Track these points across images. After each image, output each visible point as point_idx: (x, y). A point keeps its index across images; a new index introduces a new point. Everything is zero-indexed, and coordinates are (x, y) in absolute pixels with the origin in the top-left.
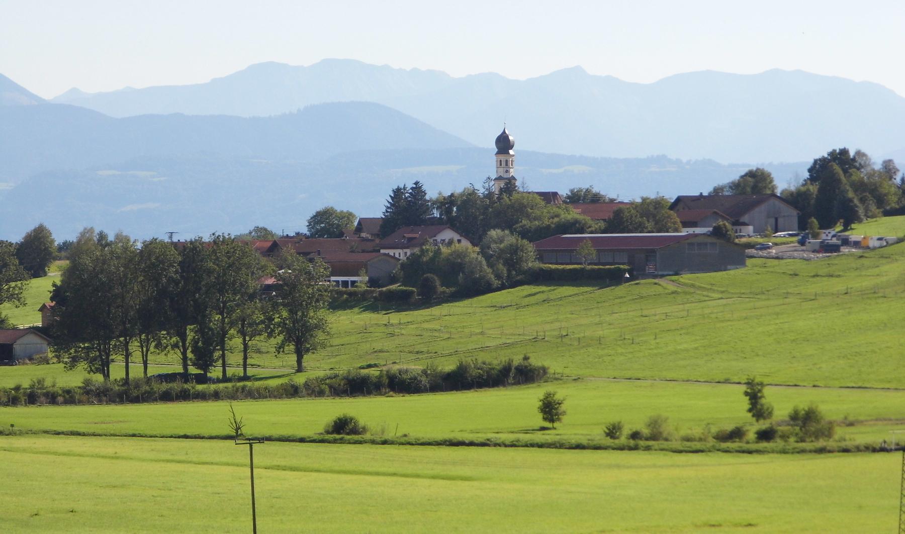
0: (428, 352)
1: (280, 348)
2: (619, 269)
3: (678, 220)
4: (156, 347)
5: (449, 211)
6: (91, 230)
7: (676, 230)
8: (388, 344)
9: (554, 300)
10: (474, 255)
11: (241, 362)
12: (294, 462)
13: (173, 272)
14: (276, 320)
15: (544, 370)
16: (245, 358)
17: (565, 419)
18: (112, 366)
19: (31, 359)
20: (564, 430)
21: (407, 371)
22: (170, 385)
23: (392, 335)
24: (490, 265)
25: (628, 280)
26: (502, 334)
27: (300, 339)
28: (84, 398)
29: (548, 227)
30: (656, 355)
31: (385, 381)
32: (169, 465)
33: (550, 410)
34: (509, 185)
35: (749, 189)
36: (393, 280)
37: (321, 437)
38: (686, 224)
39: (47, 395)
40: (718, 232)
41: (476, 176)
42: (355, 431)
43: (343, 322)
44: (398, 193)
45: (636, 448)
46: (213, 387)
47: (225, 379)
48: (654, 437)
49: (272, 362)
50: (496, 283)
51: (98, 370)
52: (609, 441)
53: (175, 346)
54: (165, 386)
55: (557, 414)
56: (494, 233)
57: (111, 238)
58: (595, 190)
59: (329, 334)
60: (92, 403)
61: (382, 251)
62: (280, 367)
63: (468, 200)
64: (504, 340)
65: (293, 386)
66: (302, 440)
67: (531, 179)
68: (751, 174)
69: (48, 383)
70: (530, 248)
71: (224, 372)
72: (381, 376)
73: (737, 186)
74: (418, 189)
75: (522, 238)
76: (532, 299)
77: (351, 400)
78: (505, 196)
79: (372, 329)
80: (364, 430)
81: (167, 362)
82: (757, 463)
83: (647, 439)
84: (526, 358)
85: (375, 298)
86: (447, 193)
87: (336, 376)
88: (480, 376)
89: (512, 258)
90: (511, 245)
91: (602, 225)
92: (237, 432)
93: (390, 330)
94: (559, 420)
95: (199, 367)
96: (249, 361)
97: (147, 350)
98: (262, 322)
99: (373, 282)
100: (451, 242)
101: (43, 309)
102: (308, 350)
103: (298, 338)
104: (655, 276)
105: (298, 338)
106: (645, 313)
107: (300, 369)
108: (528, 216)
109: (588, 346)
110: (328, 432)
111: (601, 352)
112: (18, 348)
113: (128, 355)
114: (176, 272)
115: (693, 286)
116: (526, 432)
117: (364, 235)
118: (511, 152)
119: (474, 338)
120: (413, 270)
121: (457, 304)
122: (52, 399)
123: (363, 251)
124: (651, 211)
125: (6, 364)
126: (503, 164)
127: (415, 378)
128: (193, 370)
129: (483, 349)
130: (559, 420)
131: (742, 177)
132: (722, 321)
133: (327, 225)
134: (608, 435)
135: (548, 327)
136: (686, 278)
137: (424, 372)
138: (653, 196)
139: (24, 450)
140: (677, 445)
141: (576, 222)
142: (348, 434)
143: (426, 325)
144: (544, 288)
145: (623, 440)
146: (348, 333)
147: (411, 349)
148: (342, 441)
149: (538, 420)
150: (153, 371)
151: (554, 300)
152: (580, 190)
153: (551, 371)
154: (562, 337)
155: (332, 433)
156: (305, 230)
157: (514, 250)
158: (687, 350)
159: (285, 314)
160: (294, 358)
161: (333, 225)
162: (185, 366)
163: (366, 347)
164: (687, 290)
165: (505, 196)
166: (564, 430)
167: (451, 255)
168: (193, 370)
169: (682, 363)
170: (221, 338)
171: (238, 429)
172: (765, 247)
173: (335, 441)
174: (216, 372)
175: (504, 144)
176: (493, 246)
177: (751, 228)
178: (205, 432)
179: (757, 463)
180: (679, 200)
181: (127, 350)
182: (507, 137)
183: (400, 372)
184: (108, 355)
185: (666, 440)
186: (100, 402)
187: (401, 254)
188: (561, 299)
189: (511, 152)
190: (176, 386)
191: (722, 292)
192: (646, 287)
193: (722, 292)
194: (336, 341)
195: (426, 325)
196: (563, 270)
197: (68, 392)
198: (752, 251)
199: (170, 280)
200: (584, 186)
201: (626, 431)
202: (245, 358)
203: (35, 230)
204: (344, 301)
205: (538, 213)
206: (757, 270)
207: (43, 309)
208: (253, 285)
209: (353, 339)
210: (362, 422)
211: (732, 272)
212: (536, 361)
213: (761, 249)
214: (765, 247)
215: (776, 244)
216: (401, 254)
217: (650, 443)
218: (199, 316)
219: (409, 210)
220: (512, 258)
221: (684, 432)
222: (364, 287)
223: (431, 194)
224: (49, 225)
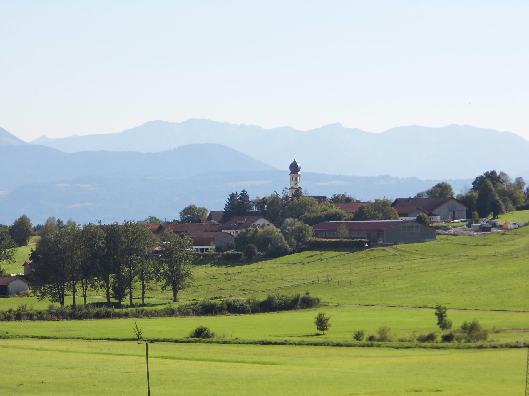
0: (250, 290)
1: (164, 288)
2: (362, 241)
3: (396, 213)
4: (91, 287)
5: (262, 207)
6: (53, 219)
7: (395, 219)
8: (227, 285)
9: (324, 259)
10: (277, 233)
11: (141, 296)
12: (172, 354)
13: (101, 243)
14: (161, 271)
15: (318, 300)
16: (143, 293)
17: (330, 329)
19: (18, 294)
20: (330, 335)
22: (100, 309)
23: (229, 280)
24: (287, 239)
25: (367, 248)
27: (175, 282)
28: (49, 316)
29: (321, 216)
31: (225, 306)
33: (322, 324)
34: (298, 192)
35: (438, 195)
36: (230, 248)
37: (187, 339)
38: (401, 215)
39: (27, 315)
40: (420, 220)
41: (278, 187)
42: (207, 336)
43: (201, 272)
45: (372, 346)
47: (132, 306)
48: (382, 339)
49: (159, 295)
50: (290, 249)
52: (356, 342)
53: (102, 286)
54: (96, 310)
55: (325, 326)
56: (289, 220)
57: (65, 223)
58: (348, 195)
59: (192, 279)
60: (53, 319)
61: (223, 231)
63: (274, 201)
65: (171, 310)
66: (177, 341)
67: (310, 189)
70: (310, 229)
71: (131, 301)
72: (222, 304)
74: (244, 195)
75: (305, 223)
77: (205, 318)
78: (295, 198)
79: (217, 276)
80: (213, 335)
81: (98, 295)
82: (442, 355)
83: (378, 341)
84: (307, 293)
85: (219, 258)
86: (261, 197)
87: (196, 304)
88: (281, 304)
89: (299, 235)
91: (352, 215)
92: (139, 336)
93: (228, 277)
94: (327, 329)
95: (116, 299)
96: (146, 295)
97: (86, 289)
98: (153, 272)
99: (218, 249)
100: (263, 226)
101: (25, 264)
102: (180, 289)
106: (377, 267)
108: (309, 210)
109: (344, 286)
111: (351, 290)
112: (10, 287)
113: (75, 292)
114: (103, 243)
115: (405, 251)
116: (308, 336)
117: (212, 221)
118: (299, 173)
119: (277, 282)
120: (242, 242)
121: (267, 262)
122: (30, 317)
123: (212, 231)
124: (381, 207)
125: (3, 297)
126: (294, 180)
127: (243, 305)
128: (113, 300)
130: (327, 329)
131: (434, 187)
133: (191, 215)
136: (401, 246)
137: (248, 301)
138: (381, 199)
139: (14, 347)
141: (337, 214)
142: (203, 338)
143: (249, 274)
144: (318, 252)
145: (364, 341)
147: (240, 288)
148: (200, 342)
149: (315, 330)
150: (89, 301)
151: (324, 259)
152: (339, 195)
153: (322, 301)
154: (329, 281)
155: (194, 337)
156: (178, 219)
157: (301, 230)
158: (401, 289)
159: (167, 268)
162: (108, 298)
163: (214, 287)
165: (295, 198)
166: (330, 335)
167: (264, 233)
168: (113, 300)
170: (129, 282)
171: (139, 334)
172: (447, 229)
173: (196, 342)
174: (126, 301)
175: (294, 168)
176: (288, 228)
177: (439, 217)
179: (442, 355)
180: (397, 201)
181: (74, 288)
182: (297, 164)
183: (234, 301)
184: (63, 292)
185: (390, 341)
186: (59, 319)
187: (235, 233)
188: (328, 259)
189: (299, 173)
190: (103, 310)
191: (422, 255)
192: (377, 251)
194: (196, 284)
195: (249, 274)
196: (329, 242)
197: (40, 313)
198: (440, 231)
199: (100, 248)
200: (342, 193)
201: (366, 336)
202: (143, 293)
203: (20, 219)
204: (201, 260)
206: (442, 241)
207: (25, 264)
209: (206, 282)
211: (428, 243)
212: (313, 295)
213: (445, 230)
214: (447, 229)
215: (454, 227)
216: (235, 233)
217: (380, 343)
218: (116, 269)
219: (239, 207)
220: (299, 235)
221: (400, 336)
222: (213, 252)
223: (252, 197)
224: (28, 216)
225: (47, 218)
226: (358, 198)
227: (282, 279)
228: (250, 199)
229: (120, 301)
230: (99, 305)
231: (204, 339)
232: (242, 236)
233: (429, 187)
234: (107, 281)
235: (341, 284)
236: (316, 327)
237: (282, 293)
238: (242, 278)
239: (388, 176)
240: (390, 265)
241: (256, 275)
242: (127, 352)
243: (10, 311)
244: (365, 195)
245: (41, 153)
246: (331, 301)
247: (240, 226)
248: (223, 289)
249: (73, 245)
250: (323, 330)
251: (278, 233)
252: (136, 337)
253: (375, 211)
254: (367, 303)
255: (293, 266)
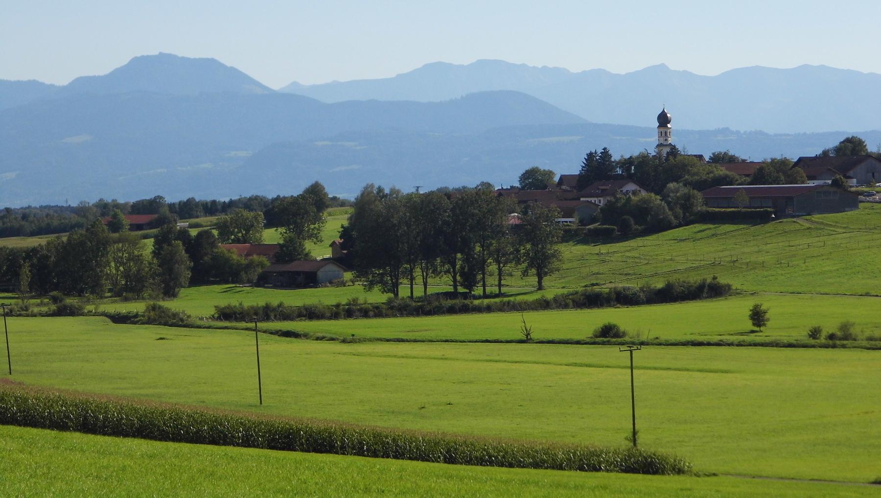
0: (634, 274)
1: (525, 273)
2: (767, 212)
3: (804, 175)
4: (433, 272)
5: (629, 169)
6: (372, 186)
7: (803, 183)
8: (603, 268)
9: (721, 234)
10: (658, 202)
11: (497, 283)
12: (586, 360)
13: (447, 215)
14: (522, 251)
15: (729, 286)
16: (500, 280)
17: (768, 324)
18: (400, 287)
19: (331, 283)
20: (768, 333)
21: (629, 288)
22: (454, 301)
23: (604, 261)
24: (671, 209)
25: (773, 219)
26: (687, 260)
27: (541, 265)
28: (390, 312)
29: (706, 181)
30: (808, 275)
31: (614, 296)
32: (537, 365)
33: (758, 317)
34: (673, 151)
35: (849, 152)
36: (593, 220)
37: (592, 340)
38: (812, 178)
39: (360, 310)
40: (836, 183)
41: (647, 144)
42: (617, 335)
43: (570, 251)
44: (590, 156)
45: (834, 346)
46: (477, 302)
47: (485, 296)
48: (846, 337)
49: (519, 283)
50: (675, 222)
51: (389, 291)
52: (812, 341)
53: (448, 271)
54: (450, 302)
55: (763, 320)
56: (672, 185)
57: (387, 191)
58: (731, 153)
59: (560, 261)
60: (395, 316)
61: (582, 199)
62: (524, 286)
63: (642, 161)
64: (689, 265)
65: (545, 301)
66: (578, 343)
67: (688, 147)
68: (848, 140)
69: (361, 301)
70: (699, 196)
71: (484, 290)
72: (610, 292)
73: (838, 150)
74: (606, 153)
75: (693, 189)
76: (699, 235)
77: (589, 310)
78: (671, 158)
79: (587, 257)
80: (624, 334)
81: (441, 284)
82: (413, 331)
83: (840, 339)
84: (715, 278)
85: (585, 234)
86: (627, 156)
87: (577, 293)
88: (683, 292)
89: (686, 203)
90: (685, 194)
91: (748, 179)
92: (527, 336)
93: (602, 257)
94: (764, 325)
95: (466, 287)
96: (503, 282)
97: (427, 275)
98: (512, 253)
99: (582, 222)
100: (634, 193)
101: (333, 245)
102: (546, 274)
103: (538, 264)
104: (793, 217)
105: (538, 264)
106: (792, 244)
107: (540, 288)
108: (688, 172)
109: (755, 268)
110: (213, 318)
111: (766, 273)
112: (320, 274)
113: (412, 279)
114: (449, 216)
115: (822, 223)
116: (742, 334)
117: (563, 187)
118: (669, 126)
119: (667, 263)
120: (611, 213)
121: (647, 238)
122: (365, 313)
123: (566, 200)
124: (780, 169)
125: (311, 287)
126: (663, 134)
127: (636, 294)
128: (461, 289)
129: (675, 271)
130: (764, 325)
131: (841, 143)
132: (852, 250)
133: (535, 181)
134: (810, 336)
135: (721, 254)
136: (816, 217)
137: (642, 289)
138: (778, 157)
139: (370, 355)
140: (865, 343)
141: (727, 176)
142: (612, 337)
143: (628, 254)
144: (711, 226)
145: (822, 340)
146: (570, 261)
147: (621, 272)
148: (609, 343)
149: (749, 325)
150: (431, 290)
151: (721, 234)
152: (720, 153)
153: (734, 288)
154: (734, 261)
155: (600, 337)
156: (517, 184)
157: (688, 198)
158: (831, 271)
159: (528, 246)
160: (534, 280)
161: (538, 180)
162: (455, 286)
163: (585, 271)
164: (818, 226)
165: (671, 158)
166: (768, 333)
167: (639, 201)
168: (461, 289)
169: (830, 281)
170: (482, 265)
171: (528, 335)
172: (870, 195)
173: (603, 343)
174: (478, 291)
175: (663, 119)
176: (671, 195)
177: (855, 180)
178: (503, 338)
179: (413, 331)
180: (801, 160)
181: (412, 275)
182: (666, 114)
183: (624, 289)
184: (397, 279)
185: (855, 340)
186: (402, 315)
187: (601, 202)
188: (725, 234)
189: (669, 126)
190: (458, 302)
191: (845, 228)
192: (787, 224)
193: (845, 228)
194: (565, 266)
195: (628, 254)
196: (724, 212)
197: (377, 308)
198: (861, 197)
199: (445, 223)
200: (722, 150)
201: (824, 334)
202: (500, 280)
203: (312, 186)
204: (569, 236)
205: (696, 170)
206: (867, 211)
207: (333, 245)
208: (152, 240)
209: (575, 264)
210: (622, 328)
211: (849, 213)
212: (723, 280)
213: (868, 196)
214: (870, 195)
215: (878, 192)
216: (601, 202)
217: (845, 342)
218: (466, 247)
219: (599, 169)
220: (686, 203)
221: (868, 333)
222: (574, 227)
223: (616, 157)
224: (322, 182)
225: (364, 185)
226: (743, 157)
227: (671, 260)
228: (613, 159)
229: (471, 289)
230: (447, 295)
231: (614, 340)
232: (610, 207)
233: (833, 143)
234: (454, 265)
235: (751, 266)
236: (750, 322)
237: (681, 278)
238: (620, 259)
239: (727, 128)
240: (809, 241)
241: (637, 255)
242: (525, 359)
243: (338, 306)
244: (754, 154)
245: (293, 102)
246: (745, 288)
247: (603, 193)
248: (598, 274)
249: (410, 218)
250: (759, 326)
251: (658, 202)
252: (524, 338)
253: (778, 172)
254: (791, 289)
255: (682, 243)
